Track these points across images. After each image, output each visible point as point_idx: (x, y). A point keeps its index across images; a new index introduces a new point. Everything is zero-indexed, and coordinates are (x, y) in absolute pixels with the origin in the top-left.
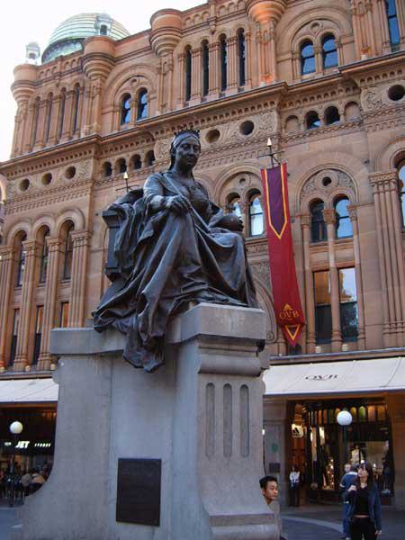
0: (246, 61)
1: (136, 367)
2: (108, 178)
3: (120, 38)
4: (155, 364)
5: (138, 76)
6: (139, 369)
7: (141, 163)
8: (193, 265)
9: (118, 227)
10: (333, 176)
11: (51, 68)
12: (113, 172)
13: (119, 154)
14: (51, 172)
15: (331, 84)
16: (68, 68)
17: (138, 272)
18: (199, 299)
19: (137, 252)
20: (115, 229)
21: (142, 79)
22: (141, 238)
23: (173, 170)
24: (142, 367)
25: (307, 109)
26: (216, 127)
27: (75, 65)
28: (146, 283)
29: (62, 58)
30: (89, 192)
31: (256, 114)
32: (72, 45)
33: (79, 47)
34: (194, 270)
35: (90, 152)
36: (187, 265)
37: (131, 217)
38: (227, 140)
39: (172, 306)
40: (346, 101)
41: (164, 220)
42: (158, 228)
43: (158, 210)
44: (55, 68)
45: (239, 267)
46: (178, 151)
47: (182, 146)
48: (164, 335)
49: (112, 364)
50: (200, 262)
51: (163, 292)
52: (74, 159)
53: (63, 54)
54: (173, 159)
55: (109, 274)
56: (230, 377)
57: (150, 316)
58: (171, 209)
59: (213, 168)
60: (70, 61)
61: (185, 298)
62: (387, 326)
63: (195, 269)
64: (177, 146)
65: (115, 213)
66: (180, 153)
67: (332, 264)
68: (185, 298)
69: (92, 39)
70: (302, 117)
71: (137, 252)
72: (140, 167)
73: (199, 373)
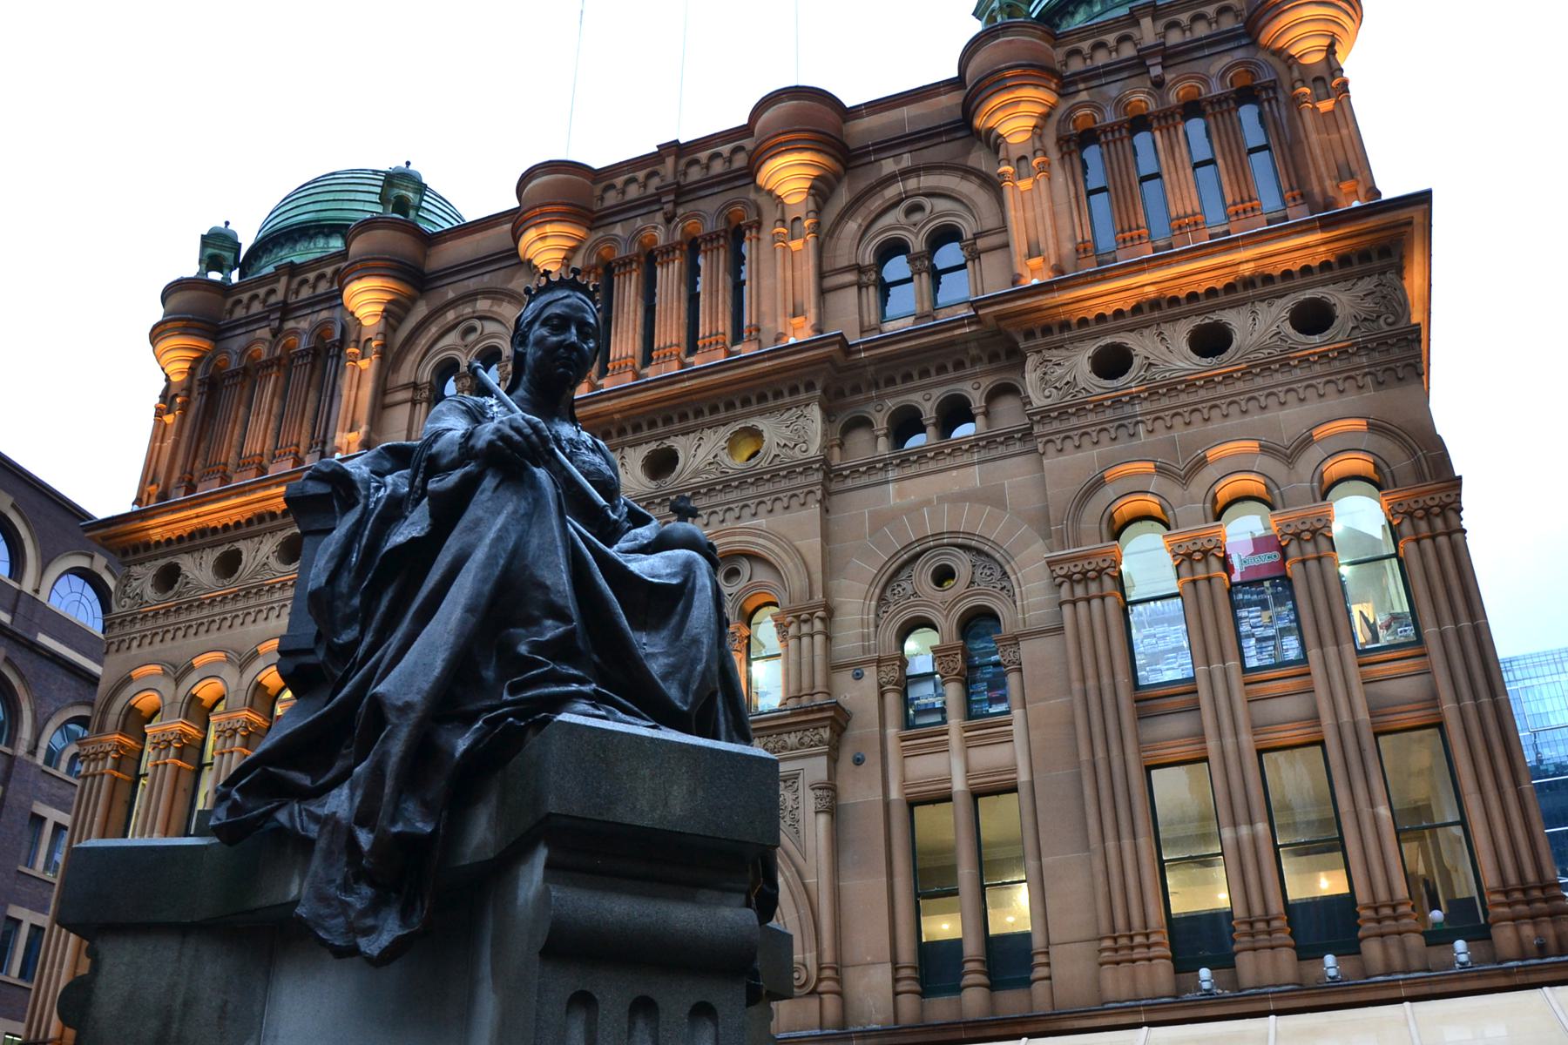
0: (746, 289)
3: (447, 226)
5: (481, 318)
10: (962, 564)
11: (262, 292)
13: (897, 394)
14: (240, 545)
15: (951, 343)
16: (305, 293)
21: (490, 327)
25: (891, 404)
26: (668, 443)
27: (323, 287)
29: (293, 270)
30: (287, 610)
31: (771, 411)
32: (321, 242)
33: (336, 244)
36: (531, 622)
38: (697, 473)
40: (987, 382)
41: (467, 489)
42: (448, 511)
44: (273, 291)
48: (435, 831)
53: (297, 260)
60: (311, 276)
62: (1108, 943)
63: (551, 630)
67: (959, 785)
69: (368, 225)
70: (881, 422)
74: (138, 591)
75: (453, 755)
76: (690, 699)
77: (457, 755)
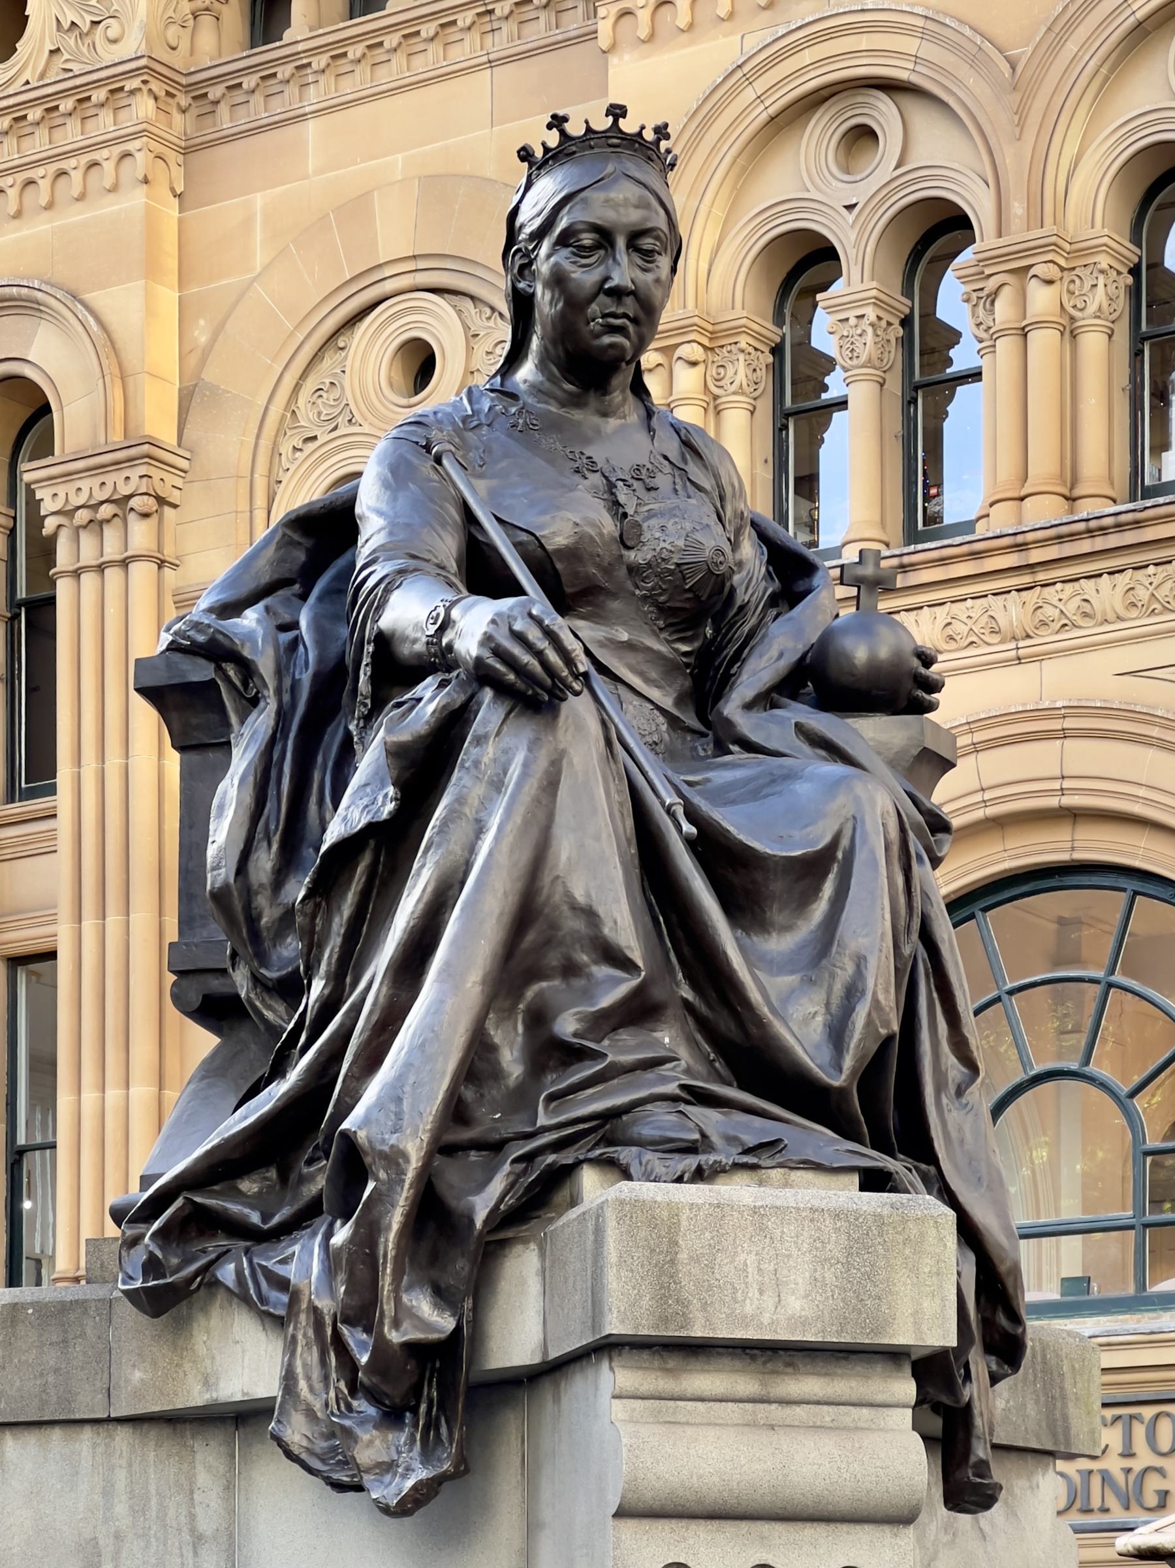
2: (269, 52)
4: (421, 1473)
6: (351, 1495)
8: (602, 971)
22: (334, 832)
23: (527, 372)
24: (359, 1488)
28: (372, 1059)
34: (606, 1000)
39: (497, 1185)
43: (414, 672)
45: (860, 962)
46: (543, 267)
48: (458, 1329)
49: (1073, 829)
50: (637, 956)
54: (522, 306)
55: (196, 1000)
57: (389, 1241)
58: (482, 675)
61: (558, 1146)
64: (539, 235)
65: (201, 671)
66: (558, 280)
68: (558, 1146)
72: (40, 1285)
73: (614, 1516)
75: (471, 1222)
76: (848, 1062)
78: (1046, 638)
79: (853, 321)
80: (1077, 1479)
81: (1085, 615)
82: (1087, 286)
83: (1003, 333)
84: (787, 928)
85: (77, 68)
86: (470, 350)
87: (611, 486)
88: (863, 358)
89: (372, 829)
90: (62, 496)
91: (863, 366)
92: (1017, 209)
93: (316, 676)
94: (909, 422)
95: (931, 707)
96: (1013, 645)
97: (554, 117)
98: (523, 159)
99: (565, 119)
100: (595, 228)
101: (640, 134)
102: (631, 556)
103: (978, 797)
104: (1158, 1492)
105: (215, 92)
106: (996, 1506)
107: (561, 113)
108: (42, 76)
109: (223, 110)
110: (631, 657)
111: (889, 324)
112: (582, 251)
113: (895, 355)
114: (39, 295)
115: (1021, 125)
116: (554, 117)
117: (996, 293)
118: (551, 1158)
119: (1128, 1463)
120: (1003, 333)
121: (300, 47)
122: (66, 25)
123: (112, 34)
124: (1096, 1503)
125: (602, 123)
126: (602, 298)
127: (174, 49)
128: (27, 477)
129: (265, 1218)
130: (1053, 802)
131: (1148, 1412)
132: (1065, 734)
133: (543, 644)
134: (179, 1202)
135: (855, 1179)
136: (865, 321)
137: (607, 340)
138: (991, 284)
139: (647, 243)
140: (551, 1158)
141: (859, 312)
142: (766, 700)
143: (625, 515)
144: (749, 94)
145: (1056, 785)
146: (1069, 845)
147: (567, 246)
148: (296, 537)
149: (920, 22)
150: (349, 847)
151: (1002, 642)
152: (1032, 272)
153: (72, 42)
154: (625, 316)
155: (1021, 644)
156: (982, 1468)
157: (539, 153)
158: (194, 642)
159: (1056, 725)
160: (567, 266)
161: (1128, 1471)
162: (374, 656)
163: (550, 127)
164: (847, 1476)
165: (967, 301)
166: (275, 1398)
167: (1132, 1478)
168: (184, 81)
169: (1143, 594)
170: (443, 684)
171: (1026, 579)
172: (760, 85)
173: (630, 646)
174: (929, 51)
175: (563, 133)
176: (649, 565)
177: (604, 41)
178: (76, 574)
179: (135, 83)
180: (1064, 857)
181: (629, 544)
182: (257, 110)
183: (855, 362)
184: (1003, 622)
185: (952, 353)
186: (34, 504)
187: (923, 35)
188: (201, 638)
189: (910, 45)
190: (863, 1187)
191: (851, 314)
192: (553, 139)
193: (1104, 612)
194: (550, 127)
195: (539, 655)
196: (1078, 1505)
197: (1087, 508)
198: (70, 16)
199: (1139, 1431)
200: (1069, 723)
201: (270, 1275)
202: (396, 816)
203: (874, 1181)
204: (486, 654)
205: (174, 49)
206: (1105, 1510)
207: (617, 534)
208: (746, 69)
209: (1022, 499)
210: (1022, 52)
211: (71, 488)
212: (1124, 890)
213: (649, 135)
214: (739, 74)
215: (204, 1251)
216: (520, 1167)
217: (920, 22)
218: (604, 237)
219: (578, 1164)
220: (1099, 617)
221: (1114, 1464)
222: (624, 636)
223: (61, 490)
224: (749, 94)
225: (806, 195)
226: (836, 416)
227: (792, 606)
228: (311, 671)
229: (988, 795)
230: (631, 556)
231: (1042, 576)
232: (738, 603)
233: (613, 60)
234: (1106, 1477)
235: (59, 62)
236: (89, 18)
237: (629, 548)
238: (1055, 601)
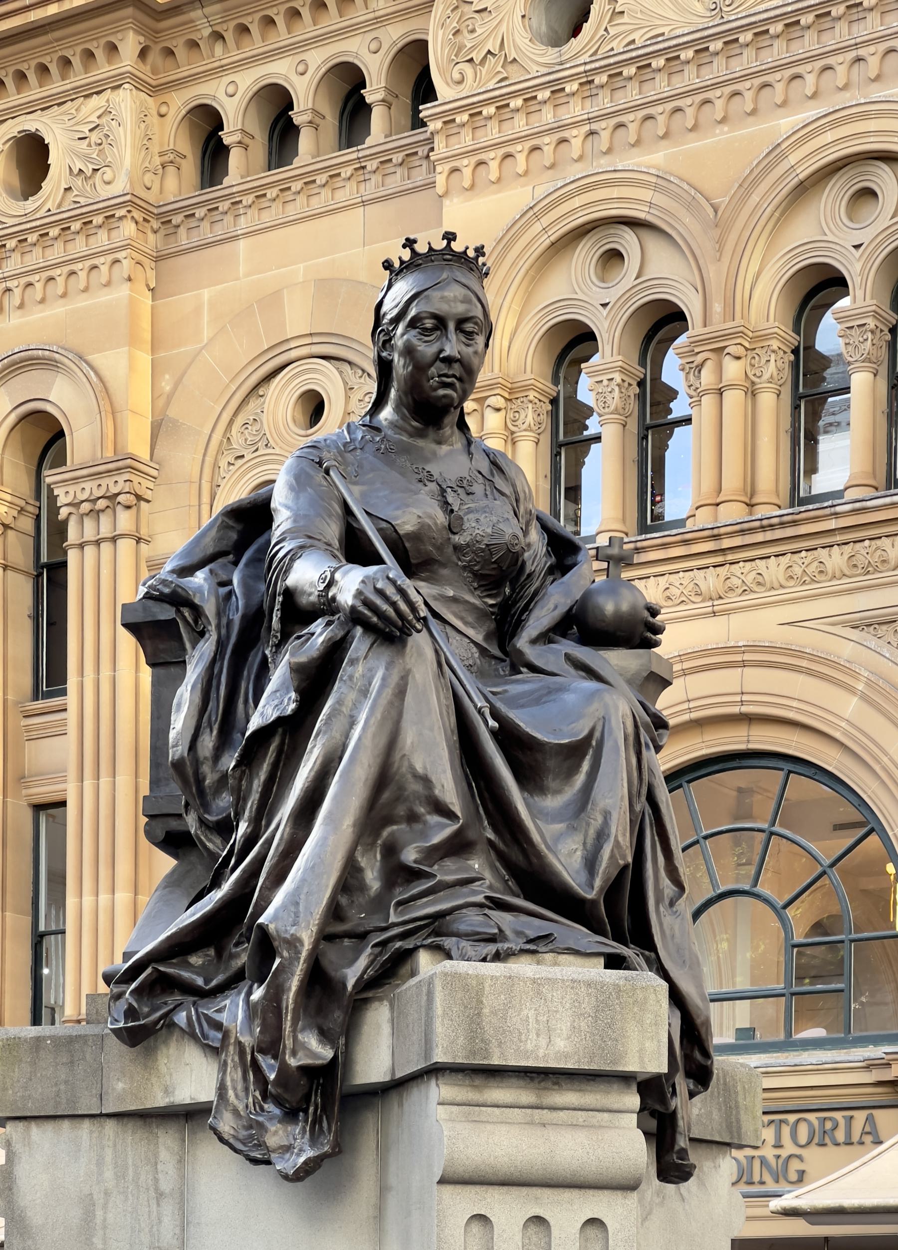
1: (255, 1161)
4: (309, 1153)
7: (368, 108)
8: (434, 819)
9: (431, 11)
12: (305, 142)
17: (250, 841)
18: (448, 942)
19: (248, 760)
20: (173, 670)
22: (255, 723)
23: (387, 413)
24: (268, 1162)
28: (279, 876)
34: (436, 839)
35: (113, 48)
37: (225, 626)
39: (362, 962)
45: (607, 815)
46: (399, 341)
47: (413, 324)
50: (457, 809)
51: (335, 912)
52: (35, 92)
54: (384, 368)
55: (161, 835)
56: (605, 1196)
57: (290, 997)
58: (355, 618)
59: (723, 134)
64: (396, 320)
66: (409, 351)
68: (403, 936)
71: (248, 760)
74: (489, 46)
76: (598, 883)
77: (350, 987)
78: (733, 599)
79: (605, 382)
80: (744, 1161)
81: (759, 584)
82: (763, 361)
83: (706, 392)
84: (558, 792)
85: (83, 201)
86: (348, 398)
87: (443, 491)
88: (612, 408)
89: (280, 721)
90: (72, 493)
91: (611, 413)
92: (717, 308)
93: (244, 617)
94: (642, 451)
95: (656, 644)
96: (710, 604)
97: (407, 239)
98: (386, 268)
99: (415, 241)
100: (435, 316)
101: (465, 252)
102: (456, 539)
103: (686, 706)
104: (798, 1171)
105: (177, 219)
106: (692, 1179)
107: (412, 237)
108: (59, 206)
109: (182, 231)
110: (455, 607)
111: (630, 385)
112: (425, 332)
113: (633, 406)
114: (57, 356)
115: (720, 251)
116: (407, 239)
117: (702, 365)
118: (398, 944)
119: (778, 1152)
120: (706, 392)
121: (234, 189)
122: (76, 171)
123: (107, 177)
124: (756, 1178)
125: (441, 244)
126: (438, 363)
127: (149, 189)
128: (48, 480)
129: (207, 982)
130: (736, 710)
131: (792, 1118)
132: (744, 664)
133: (397, 598)
134: (149, 970)
135: (602, 961)
136: (614, 383)
137: (441, 392)
138: (699, 359)
139: (469, 327)
140: (398, 944)
141: (610, 376)
142: (545, 638)
143: (452, 511)
144: (538, 227)
145: (738, 698)
146: (746, 739)
147: (415, 328)
148: (231, 523)
149: (654, 180)
150: (265, 733)
151: (703, 601)
152: (726, 351)
153: (80, 183)
154: (454, 376)
155: (716, 603)
156: (683, 1153)
157: (397, 264)
158: (162, 593)
159: (739, 658)
160: (415, 341)
161: (778, 1157)
162: (283, 604)
163: (404, 246)
164: (593, 1158)
165: (683, 370)
166: (212, 1102)
167: (780, 1161)
168: (156, 211)
169: (798, 570)
170: (329, 624)
171: (719, 559)
172: (545, 221)
173: (454, 600)
174: (660, 199)
175: (413, 251)
176: (468, 545)
177: (440, 188)
178: (81, 546)
179: (122, 212)
180: (742, 747)
181: (455, 531)
182: (206, 232)
183: (607, 410)
184: (703, 587)
185: (672, 405)
186: (53, 499)
187: (656, 188)
188: (167, 590)
189: (646, 195)
190: (606, 967)
191: (604, 378)
192: (406, 255)
193: (772, 582)
194: (404, 246)
195: (393, 604)
196: (744, 1179)
197: (761, 512)
198: (78, 165)
199: (786, 1131)
200: (747, 657)
201: (209, 1020)
202: (296, 712)
203: (614, 962)
204: (358, 603)
205: (149, 189)
206: (762, 1183)
207: (446, 524)
208: (536, 210)
209: (718, 505)
210: (722, 201)
211: (79, 488)
212: (782, 770)
213: (471, 253)
214: (531, 213)
215: (166, 1003)
216: (378, 950)
217: (654, 180)
218: (440, 322)
219: (416, 949)
220: (768, 586)
221: (768, 1152)
222: (451, 593)
223: (71, 489)
224: (538, 227)
225: (825, 238)
226: (594, 447)
227: (563, 575)
228: (240, 613)
229: (692, 705)
230: (456, 539)
231: (730, 557)
232: (528, 571)
233: (446, 202)
234: (763, 1161)
235: (71, 197)
236: (91, 167)
237: (455, 533)
238: (739, 574)
